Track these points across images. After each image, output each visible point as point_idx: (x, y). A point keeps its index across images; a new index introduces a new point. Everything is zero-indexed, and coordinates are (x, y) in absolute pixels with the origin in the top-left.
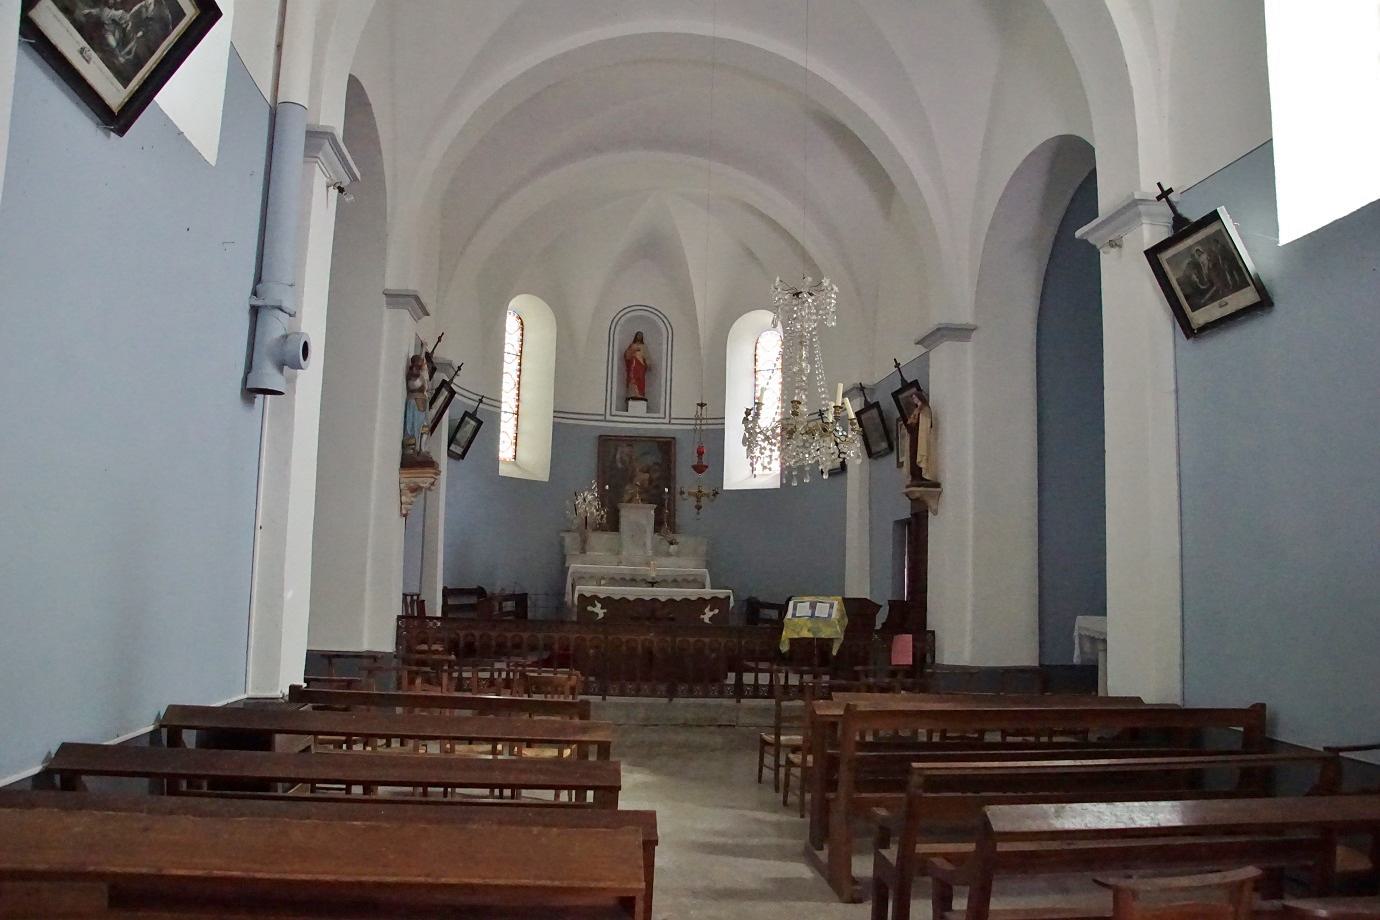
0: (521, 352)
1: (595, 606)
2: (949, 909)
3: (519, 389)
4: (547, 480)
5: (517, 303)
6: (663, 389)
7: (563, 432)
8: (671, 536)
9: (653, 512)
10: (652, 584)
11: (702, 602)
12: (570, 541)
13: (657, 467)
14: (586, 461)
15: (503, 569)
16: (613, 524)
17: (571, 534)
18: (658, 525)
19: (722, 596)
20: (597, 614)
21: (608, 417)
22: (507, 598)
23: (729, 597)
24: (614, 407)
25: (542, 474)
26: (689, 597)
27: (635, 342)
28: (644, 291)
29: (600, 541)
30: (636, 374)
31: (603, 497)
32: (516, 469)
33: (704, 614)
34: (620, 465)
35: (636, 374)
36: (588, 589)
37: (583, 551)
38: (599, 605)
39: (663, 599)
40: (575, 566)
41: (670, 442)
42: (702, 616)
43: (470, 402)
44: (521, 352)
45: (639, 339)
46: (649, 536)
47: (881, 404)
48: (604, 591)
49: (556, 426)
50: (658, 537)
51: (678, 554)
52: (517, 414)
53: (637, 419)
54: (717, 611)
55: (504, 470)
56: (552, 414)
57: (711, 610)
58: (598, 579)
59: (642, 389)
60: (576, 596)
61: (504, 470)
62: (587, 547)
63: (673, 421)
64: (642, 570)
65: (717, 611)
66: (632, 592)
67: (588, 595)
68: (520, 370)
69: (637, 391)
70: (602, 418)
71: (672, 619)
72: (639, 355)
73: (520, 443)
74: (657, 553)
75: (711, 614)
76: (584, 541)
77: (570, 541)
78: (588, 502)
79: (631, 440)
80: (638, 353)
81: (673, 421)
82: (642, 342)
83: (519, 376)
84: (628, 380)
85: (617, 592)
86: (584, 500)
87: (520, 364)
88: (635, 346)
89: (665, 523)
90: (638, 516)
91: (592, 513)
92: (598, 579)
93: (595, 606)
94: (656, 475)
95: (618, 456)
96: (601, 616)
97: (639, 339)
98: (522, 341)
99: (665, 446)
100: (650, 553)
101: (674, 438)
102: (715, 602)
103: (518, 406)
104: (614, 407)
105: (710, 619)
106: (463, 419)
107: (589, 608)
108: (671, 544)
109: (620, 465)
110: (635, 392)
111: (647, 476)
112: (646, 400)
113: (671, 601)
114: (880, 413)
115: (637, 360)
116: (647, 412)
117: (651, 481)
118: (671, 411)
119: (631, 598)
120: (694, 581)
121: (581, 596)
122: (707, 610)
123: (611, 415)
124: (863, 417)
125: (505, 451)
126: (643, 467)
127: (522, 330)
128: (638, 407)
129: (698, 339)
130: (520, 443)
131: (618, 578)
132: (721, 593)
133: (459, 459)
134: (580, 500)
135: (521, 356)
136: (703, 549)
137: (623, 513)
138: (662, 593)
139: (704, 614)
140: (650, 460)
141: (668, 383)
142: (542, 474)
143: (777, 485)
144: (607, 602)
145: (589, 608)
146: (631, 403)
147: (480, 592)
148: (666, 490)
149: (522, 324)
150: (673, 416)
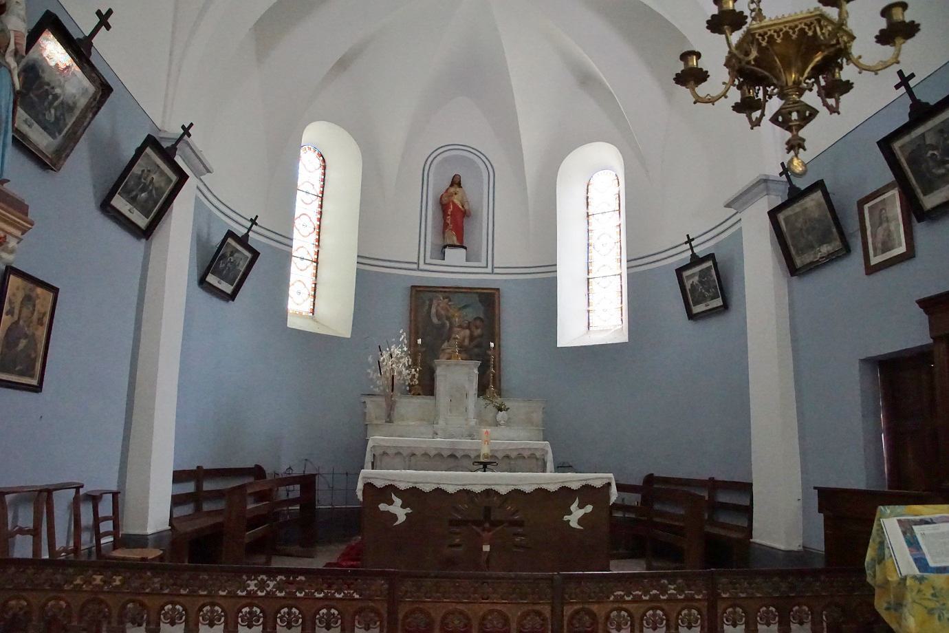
0: (322, 193)
1: (391, 502)
2: (586, 614)
3: (319, 234)
4: (349, 336)
5: (314, 133)
6: (484, 232)
7: (368, 282)
8: (499, 400)
9: (476, 371)
10: (485, 466)
11: (566, 494)
12: (374, 408)
13: (478, 323)
14: (397, 310)
15: (277, 436)
16: (426, 386)
17: (374, 399)
18: (482, 390)
19: (598, 484)
20: (395, 517)
21: (422, 266)
22: (289, 481)
23: (609, 484)
24: (428, 254)
25: (344, 330)
26: (544, 487)
27: (452, 185)
28: (465, 127)
29: (410, 406)
30: (454, 220)
31: (414, 352)
32: (311, 322)
33: (570, 513)
34: (435, 320)
35: (454, 220)
36: (380, 476)
37: (389, 419)
38: (398, 502)
39: (503, 490)
40: (377, 439)
41: (492, 295)
42: (566, 518)
43: (243, 228)
44: (322, 193)
45: (456, 182)
46: (471, 400)
47: (826, 183)
48: (404, 477)
49: (360, 273)
50: (482, 402)
51: (508, 423)
52: (317, 262)
53: (455, 269)
54: (589, 508)
55: (293, 323)
56: (355, 259)
57: (581, 506)
58: (412, 459)
59: (460, 233)
60: (360, 486)
61: (293, 323)
62: (395, 414)
63: (496, 271)
64: (466, 444)
65: (589, 508)
66: (453, 480)
67: (379, 484)
68: (321, 213)
69: (455, 238)
70: (415, 266)
71: (520, 524)
72: (456, 200)
73: (315, 290)
74: (481, 420)
75: (581, 512)
76: (391, 407)
77: (374, 408)
78: (397, 357)
79: (450, 292)
80: (456, 197)
81: (496, 271)
82: (459, 185)
83: (320, 220)
84: (445, 226)
85: (428, 479)
86: (391, 356)
87: (321, 207)
88: (452, 190)
89: (489, 383)
90: (457, 376)
91: (400, 373)
92: (412, 459)
93: (391, 502)
94: (478, 332)
95: (433, 310)
96: (402, 518)
97: (456, 182)
98: (324, 180)
99: (488, 299)
100: (473, 422)
101: (498, 289)
102: (587, 493)
103: (318, 253)
104: (428, 254)
105: (580, 521)
106: (140, 151)
107: (383, 507)
108: (500, 410)
109: (435, 320)
110: (455, 241)
111: (467, 332)
112: (465, 248)
113: (517, 493)
114: (826, 195)
115: (454, 204)
116: (467, 260)
117: (472, 338)
118: (496, 258)
119: (451, 489)
120: (532, 456)
121: (369, 486)
122: (574, 507)
123: (425, 263)
124: (781, 217)
125: (298, 302)
126: (460, 324)
127: (325, 168)
128: (455, 256)
129: (525, 189)
130: (315, 290)
131: (432, 453)
132: (597, 479)
133: (228, 301)
134: (386, 355)
135: (322, 198)
136: (538, 416)
137: (439, 372)
138: (502, 481)
139: (570, 513)
140: (470, 314)
141: (490, 252)
142: (344, 330)
143: (623, 338)
144: (412, 496)
145: (383, 507)
146: (447, 251)
147: (258, 472)
148: (492, 345)
149: (324, 160)
150: (495, 266)
